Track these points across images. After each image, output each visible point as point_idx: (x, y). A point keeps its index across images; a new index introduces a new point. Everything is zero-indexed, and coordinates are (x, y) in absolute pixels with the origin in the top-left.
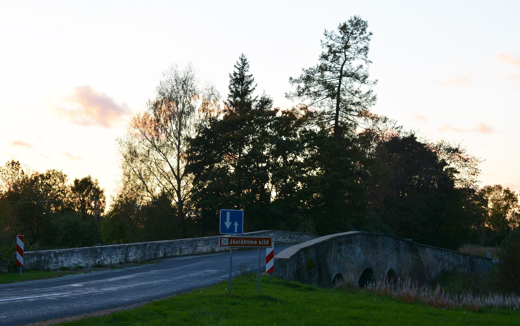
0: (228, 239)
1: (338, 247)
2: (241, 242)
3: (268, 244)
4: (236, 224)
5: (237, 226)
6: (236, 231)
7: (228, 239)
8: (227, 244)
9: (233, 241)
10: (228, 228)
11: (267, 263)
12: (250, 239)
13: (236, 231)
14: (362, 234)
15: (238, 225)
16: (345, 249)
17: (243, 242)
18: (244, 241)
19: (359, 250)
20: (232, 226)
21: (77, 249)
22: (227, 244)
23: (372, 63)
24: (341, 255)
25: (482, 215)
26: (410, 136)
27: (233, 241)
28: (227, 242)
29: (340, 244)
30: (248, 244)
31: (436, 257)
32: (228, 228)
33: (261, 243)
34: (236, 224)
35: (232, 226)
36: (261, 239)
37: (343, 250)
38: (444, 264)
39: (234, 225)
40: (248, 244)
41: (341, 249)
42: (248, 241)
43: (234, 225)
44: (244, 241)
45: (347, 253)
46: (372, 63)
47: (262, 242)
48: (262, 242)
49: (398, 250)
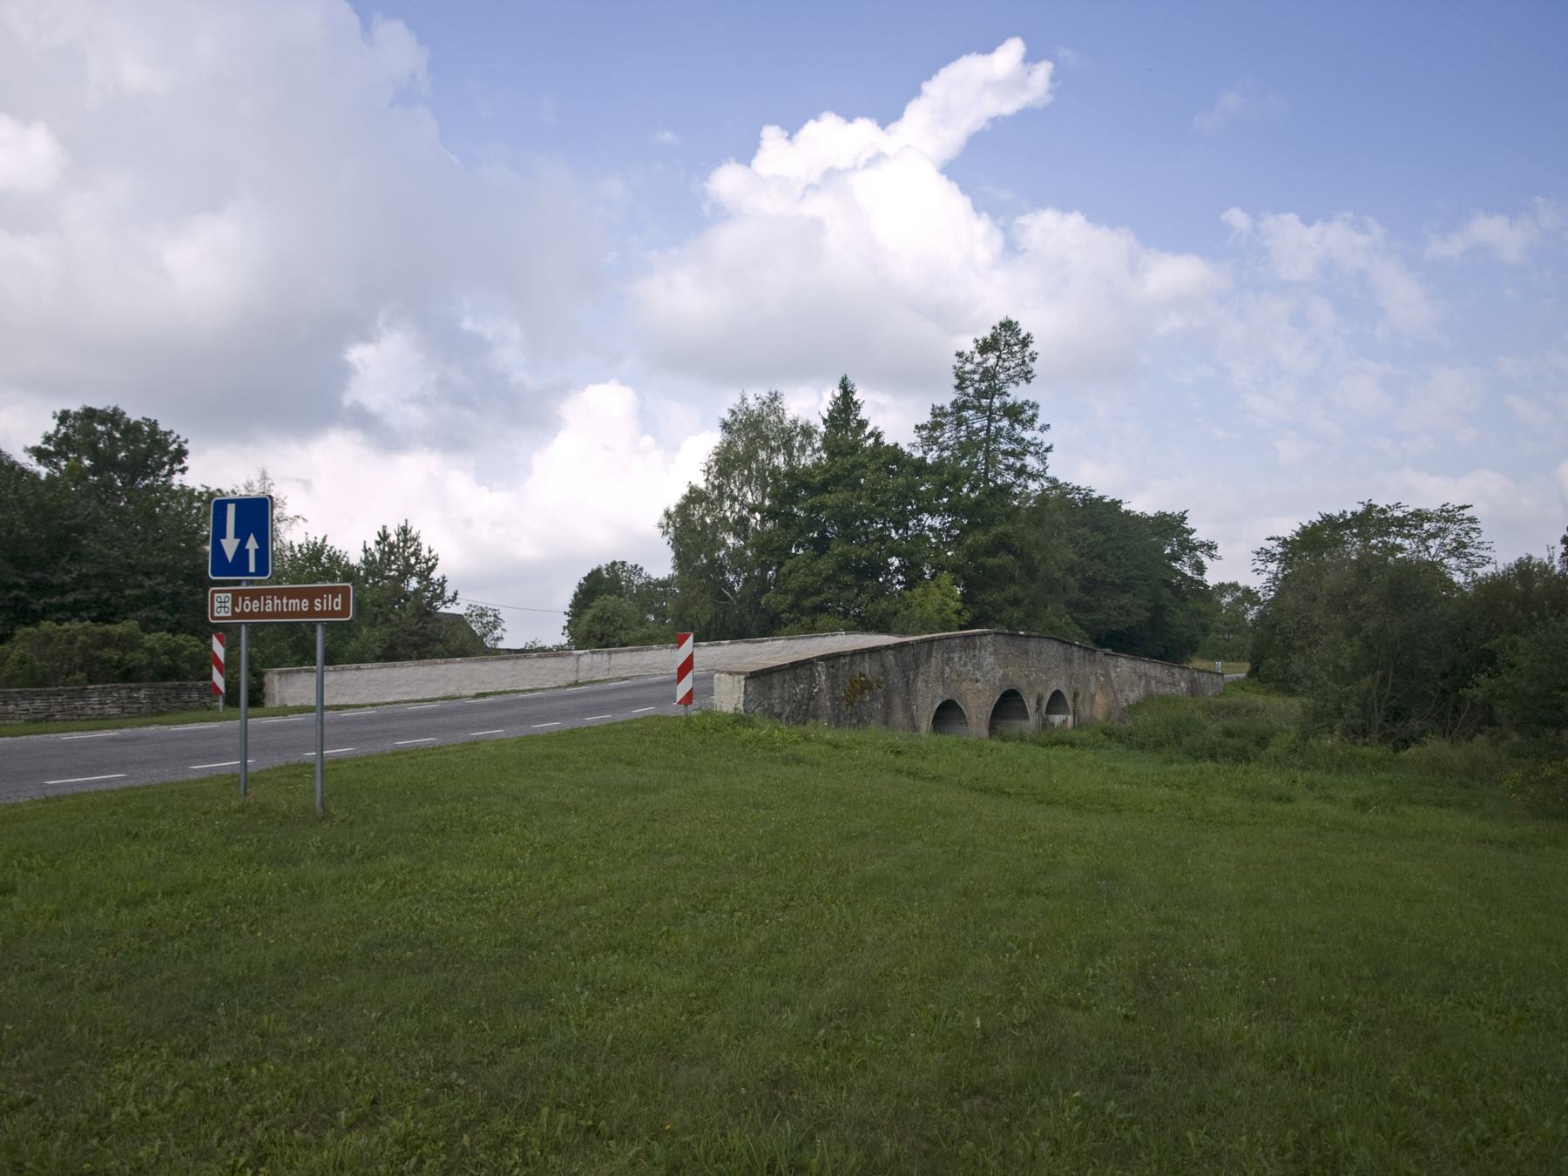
0: (230, 595)
1: (946, 655)
2: (265, 605)
3: (339, 608)
4: (252, 545)
5: (224, 537)
6: (252, 569)
7: (230, 595)
8: (229, 614)
9: (243, 601)
10: (230, 560)
11: (692, 690)
12: (291, 594)
13: (252, 569)
14: (996, 634)
15: (223, 541)
16: (960, 658)
17: (270, 605)
18: (272, 600)
19: (989, 660)
20: (242, 552)
21: (143, 684)
22: (229, 614)
23: (844, 379)
24: (951, 668)
25: (965, 518)
26: (877, 435)
27: (243, 601)
28: (229, 605)
29: (950, 650)
30: (285, 610)
31: (1135, 672)
32: (230, 560)
33: (319, 605)
34: (252, 545)
35: (242, 552)
36: (319, 593)
37: (956, 659)
38: (1148, 682)
39: (238, 541)
40: (285, 610)
41: (953, 658)
42: (285, 601)
43: (238, 541)
44: (272, 600)
45: (965, 665)
46: (844, 379)
47: (322, 603)
48: (322, 603)
49: (1069, 661)
